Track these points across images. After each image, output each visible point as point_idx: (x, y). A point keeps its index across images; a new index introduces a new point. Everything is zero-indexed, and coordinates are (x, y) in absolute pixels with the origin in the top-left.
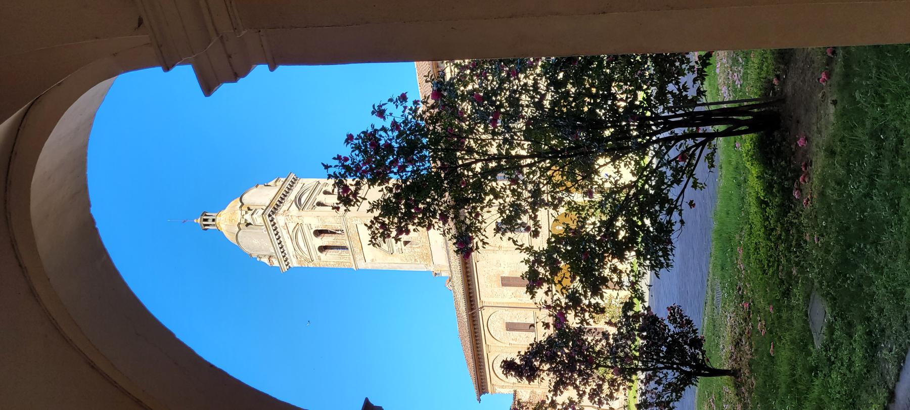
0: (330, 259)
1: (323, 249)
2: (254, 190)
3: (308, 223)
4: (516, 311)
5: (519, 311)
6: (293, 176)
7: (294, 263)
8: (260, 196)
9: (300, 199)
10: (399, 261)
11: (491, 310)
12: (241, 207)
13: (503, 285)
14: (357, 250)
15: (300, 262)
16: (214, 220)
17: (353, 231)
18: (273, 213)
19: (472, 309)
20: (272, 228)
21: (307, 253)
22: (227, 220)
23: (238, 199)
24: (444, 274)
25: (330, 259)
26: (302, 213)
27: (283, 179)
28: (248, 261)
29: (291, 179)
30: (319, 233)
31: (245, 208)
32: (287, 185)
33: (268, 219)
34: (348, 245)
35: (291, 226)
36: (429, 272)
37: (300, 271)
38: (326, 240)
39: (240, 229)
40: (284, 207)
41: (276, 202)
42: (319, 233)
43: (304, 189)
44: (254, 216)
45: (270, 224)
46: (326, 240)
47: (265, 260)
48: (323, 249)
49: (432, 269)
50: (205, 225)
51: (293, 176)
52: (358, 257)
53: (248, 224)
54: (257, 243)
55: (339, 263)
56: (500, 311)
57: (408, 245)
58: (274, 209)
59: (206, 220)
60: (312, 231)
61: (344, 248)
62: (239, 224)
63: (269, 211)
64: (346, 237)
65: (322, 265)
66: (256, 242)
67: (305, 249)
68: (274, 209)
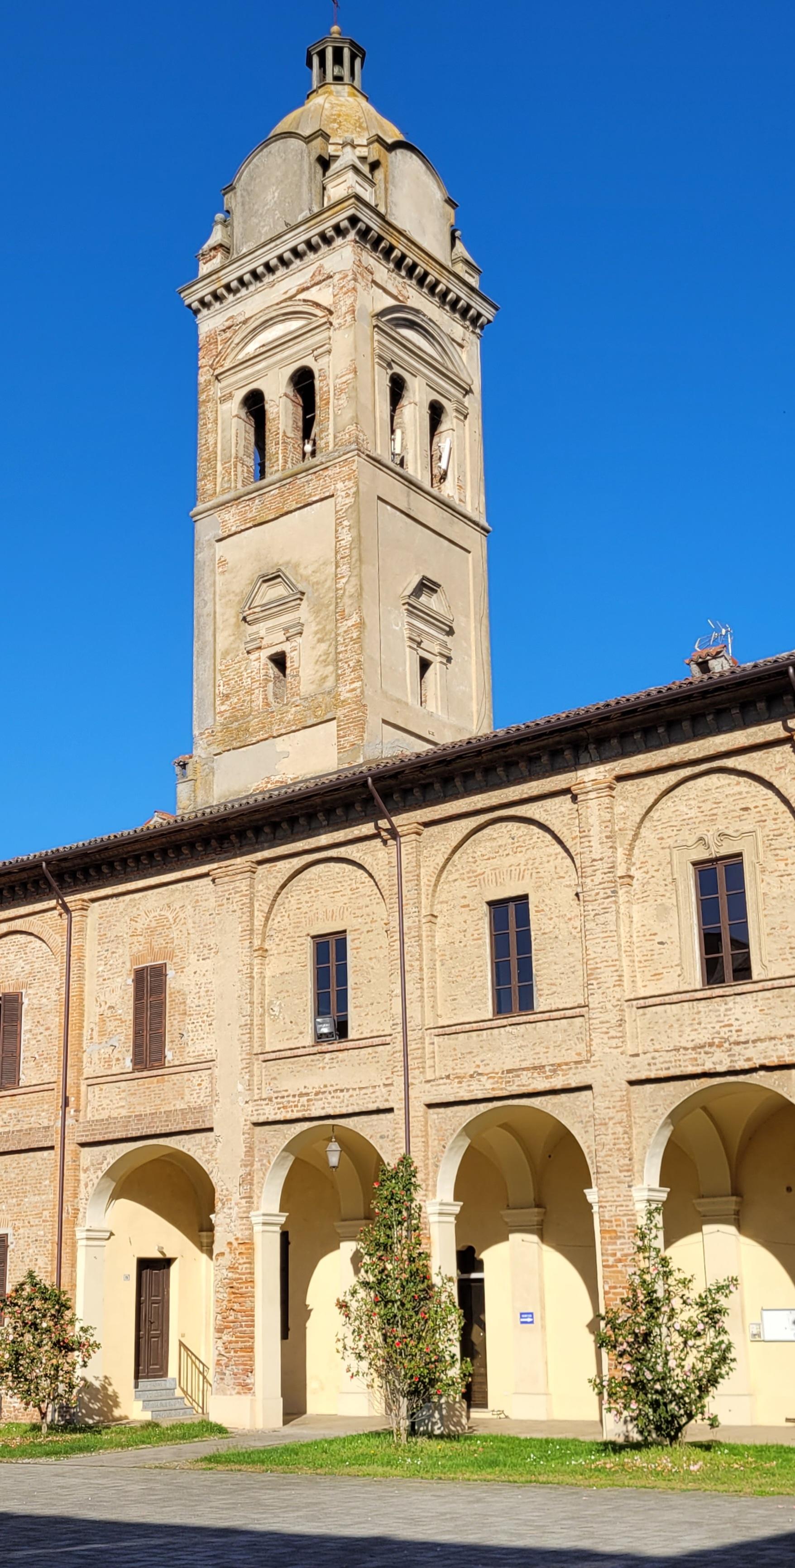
0: (223, 428)
1: (255, 403)
2: (435, 192)
3: (335, 346)
4: (56, 1021)
5: (57, 1032)
6: (488, 313)
7: (209, 323)
8: (416, 201)
9: (411, 325)
10: (221, 646)
11: (58, 941)
12: (379, 140)
13: (140, 976)
14: (254, 509)
15: (212, 339)
16: (338, 79)
17: (312, 487)
18: (364, 234)
19: (60, 877)
20: (313, 233)
21: (241, 356)
22: (341, 109)
23: (401, 137)
24: (183, 790)
25: (223, 428)
26: (366, 325)
27: (474, 282)
28: (210, 191)
29: (478, 306)
30: (304, 383)
31: (375, 152)
32: (457, 290)
33: (341, 217)
34: (269, 479)
35: (323, 295)
36: (190, 742)
37: (188, 345)
38: (281, 411)
39: (308, 140)
40: (383, 272)
41: (390, 239)
42: (304, 383)
43: (446, 343)
44: (351, 175)
45: (327, 226)
46: (281, 411)
47: (217, 235)
48: (255, 403)
49: (200, 751)
50: (322, 55)
51: (488, 313)
52: (231, 518)
53: (325, 163)
54: (271, 191)
55: (211, 461)
56: (57, 969)
57: (273, 670)
58: (377, 238)
59: (338, 59)
60: (309, 362)
61: (262, 472)
62: (326, 137)
63: (367, 218)
64: (291, 468)
65: (206, 411)
66: (272, 195)
67: (252, 348)
68: (377, 238)
